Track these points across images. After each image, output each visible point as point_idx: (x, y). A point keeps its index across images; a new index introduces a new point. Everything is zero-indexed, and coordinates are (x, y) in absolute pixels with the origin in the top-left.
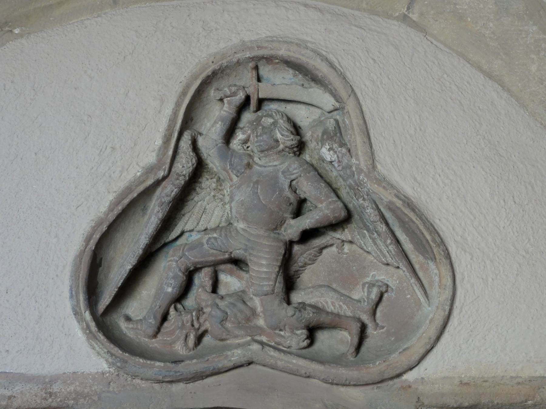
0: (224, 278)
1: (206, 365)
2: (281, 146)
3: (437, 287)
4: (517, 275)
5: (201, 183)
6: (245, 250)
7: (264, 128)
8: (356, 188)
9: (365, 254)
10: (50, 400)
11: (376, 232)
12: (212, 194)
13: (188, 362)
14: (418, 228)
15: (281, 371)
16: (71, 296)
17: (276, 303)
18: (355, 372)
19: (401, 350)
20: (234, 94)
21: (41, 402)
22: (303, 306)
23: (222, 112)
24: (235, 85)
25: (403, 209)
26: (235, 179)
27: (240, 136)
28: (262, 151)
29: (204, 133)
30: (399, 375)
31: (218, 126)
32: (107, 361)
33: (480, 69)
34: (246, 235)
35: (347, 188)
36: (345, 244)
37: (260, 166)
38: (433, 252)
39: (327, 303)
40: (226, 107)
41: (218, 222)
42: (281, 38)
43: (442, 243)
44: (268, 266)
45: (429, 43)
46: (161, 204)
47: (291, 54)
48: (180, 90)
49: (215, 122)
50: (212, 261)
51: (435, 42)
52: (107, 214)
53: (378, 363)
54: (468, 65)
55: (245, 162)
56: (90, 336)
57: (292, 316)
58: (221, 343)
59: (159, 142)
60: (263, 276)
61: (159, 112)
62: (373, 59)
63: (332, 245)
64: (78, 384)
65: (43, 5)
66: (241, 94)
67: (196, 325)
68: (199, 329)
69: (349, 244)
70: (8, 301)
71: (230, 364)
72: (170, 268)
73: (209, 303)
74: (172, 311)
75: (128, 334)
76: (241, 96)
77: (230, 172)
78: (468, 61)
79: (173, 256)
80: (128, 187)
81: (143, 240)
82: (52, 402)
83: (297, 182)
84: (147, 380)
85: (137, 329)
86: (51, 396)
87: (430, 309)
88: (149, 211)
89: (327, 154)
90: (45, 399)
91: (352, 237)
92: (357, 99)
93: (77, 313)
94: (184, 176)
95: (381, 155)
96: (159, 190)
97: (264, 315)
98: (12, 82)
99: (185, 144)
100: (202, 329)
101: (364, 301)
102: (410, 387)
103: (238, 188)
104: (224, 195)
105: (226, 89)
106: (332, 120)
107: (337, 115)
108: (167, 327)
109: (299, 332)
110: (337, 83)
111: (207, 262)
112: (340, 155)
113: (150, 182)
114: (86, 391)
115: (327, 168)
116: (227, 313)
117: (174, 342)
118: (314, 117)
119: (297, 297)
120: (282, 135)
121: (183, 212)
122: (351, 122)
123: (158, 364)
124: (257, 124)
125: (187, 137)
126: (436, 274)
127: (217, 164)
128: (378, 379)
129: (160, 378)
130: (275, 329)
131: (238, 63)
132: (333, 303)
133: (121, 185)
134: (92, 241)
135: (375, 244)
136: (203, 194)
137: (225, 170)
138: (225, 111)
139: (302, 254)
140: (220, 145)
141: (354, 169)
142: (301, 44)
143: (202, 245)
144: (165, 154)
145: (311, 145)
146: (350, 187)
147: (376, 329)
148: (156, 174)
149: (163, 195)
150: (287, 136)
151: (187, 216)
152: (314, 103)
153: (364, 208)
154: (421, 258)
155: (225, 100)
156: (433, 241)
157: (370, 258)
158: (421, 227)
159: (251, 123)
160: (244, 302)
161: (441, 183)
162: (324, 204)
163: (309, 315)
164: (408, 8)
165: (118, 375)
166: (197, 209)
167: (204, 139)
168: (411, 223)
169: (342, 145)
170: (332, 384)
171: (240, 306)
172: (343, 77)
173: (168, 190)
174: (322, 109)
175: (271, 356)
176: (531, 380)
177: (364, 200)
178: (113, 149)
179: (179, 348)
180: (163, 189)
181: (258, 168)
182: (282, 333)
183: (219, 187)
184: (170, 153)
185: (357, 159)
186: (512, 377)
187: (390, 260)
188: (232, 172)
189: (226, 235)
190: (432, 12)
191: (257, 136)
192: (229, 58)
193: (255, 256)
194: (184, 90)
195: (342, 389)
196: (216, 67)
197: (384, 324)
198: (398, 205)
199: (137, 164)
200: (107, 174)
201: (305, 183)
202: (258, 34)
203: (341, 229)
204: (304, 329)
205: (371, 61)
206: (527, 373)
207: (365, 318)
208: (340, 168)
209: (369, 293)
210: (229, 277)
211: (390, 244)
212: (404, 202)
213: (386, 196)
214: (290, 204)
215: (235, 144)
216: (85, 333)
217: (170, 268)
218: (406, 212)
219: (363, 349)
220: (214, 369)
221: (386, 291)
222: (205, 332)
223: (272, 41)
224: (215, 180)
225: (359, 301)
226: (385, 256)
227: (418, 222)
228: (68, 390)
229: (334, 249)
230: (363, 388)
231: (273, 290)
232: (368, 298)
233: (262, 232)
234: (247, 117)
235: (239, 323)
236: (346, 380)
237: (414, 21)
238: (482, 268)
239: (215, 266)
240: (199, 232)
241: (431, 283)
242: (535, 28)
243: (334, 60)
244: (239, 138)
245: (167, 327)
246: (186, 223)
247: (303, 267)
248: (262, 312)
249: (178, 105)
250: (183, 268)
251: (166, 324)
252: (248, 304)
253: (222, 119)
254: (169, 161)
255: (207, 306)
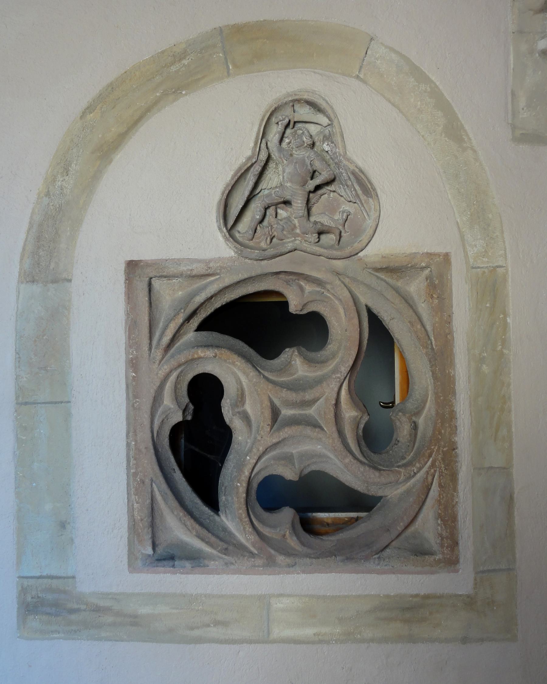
0: (279, 211)
1: (277, 251)
2: (306, 145)
3: (373, 210)
4: (405, 204)
5: (269, 165)
6: (291, 196)
7: (298, 135)
8: (338, 164)
9: (340, 197)
10: (209, 270)
11: (346, 185)
12: (274, 170)
13: (269, 250)
14: (365, 182)
15: (308, 253)
16: (217, 221)
17: (305, 220)
18: (340, 253)
19: (358, 241)
20: (284, 119)
21: (205, 272)
22: (316, 223)
23: (278, 129)
24: (284, 115)
25: (359, 173)
26: (285, 162)
27: (287, 140)
28: (297, 147)
29: (270, 140)
30: (357, 254)
31: (277, 136)
32: (234, 251)
33: (390, 102)
34: (291, 189)
35: (334, 164)
36: (331, 193)
37: (297, 155)
38: (371, 194)
39: (324, 221)
40: (280, 126)
41: (276, 185)
42: (305, 89)
43: (374, 190)
44: (301, 203)
45: (368, 89)
46: (254, 175)
47: (309, 97)
48: (261, 118)
49: (275, 134)
50: (276, 202)
51: (371, 89)
52: (230, 181)
53: (349, 248)
54: (385, 100)
55: (290, 153)
56: (226, 239)
57: (312, 227)
58: (281, 242)
59: (252, 145)
60: (299, 208)
61: (252, 130)
62: (345, 99)
63: (326, 193)
64: (221, 262)
65: (195, 78)
66: (287, 119)
67: (271, 234)
68: (272, 235)
69: (333, 192)
70: (188, 225)
71: (288, 250)
72: (257, 207)
73: (275, 223)
74: (258, 228)
75: (240, 240)
76: (287, 120)
77: (283, 159)
78: (384, 97)
79: (259, 201)
80: (239, 167)
81: (247, 193)
82: (210, 271)
83: (313, 162)
84: (251, 259)
85: (244, 236)
86: (209, 269)
87: (370, 221)
88: (247, 180)
89: (326, 147)
90: (207, 270)
91: (335, 189)
92: (338, 119)
93: (220, 229)
94: (264, 161)
95: (349, 148)
96: (252, 169)
97: (300, 227)
98: (184, 118)
99: (263, 146)
100: (273, 235)
101: (340, 220)
102: (361, 259)
103: (287, 166)
104: (279, 171)
105: (280, 117)
106: (327, 130)
107: (329, 128)
108: (257, 235)
109: (314, 235)
110: (330, 112)
111: (274, 203)
112: (332, 148)
113: (249, 164)
114: (225, 265)
115: (325, 155)
116: (284, 227)
117: (261, 242)
118: (317, 130)
119: (312, 219)
120: (306, 139)
121: (261, 180)
122: (336, 131)
123: (256, 251)
124: (295, 134)
125: (264, 141)
126: (373, 204)
127: (277, 155)
128: (349, 255)
129: (257, 258)
130: (304, 234)
131: (286, 103)
132: (327, 221)
133: (236, 167)
134: (225, 194)
135: (345, 191)
136: (270, 170)
137: (280, 158)
138: (280, 128)
139: (313, 198)
140: (278, 145)
141: (338, 154)
142: (314, 92)
143: (272, 194)
144: (255, 150)
145: (317, 144)
146: (336, 163)
147: (345, 233)
148: (252, 161)
149: (255, 171)
150: (309, 139)
151: (263, 181)
152: (319, 122)
153: (342, 173)
154: (365, 197)
155: (280, 123)
156: (371, 188)
157: (342, 199)
158: (367, 182)
159: (292, 133)
160: (291, 222)
161: (373, 160)
162: (325, 172)
163: (319, 226)
164: (359, 72)
165: (238, 258)
166: (267, 178)
167: (271, 143)
168: (362, 180)
169: (332, 142)
170: (330, 258)
171: (289, 223)
172: (332, 108)
173: (257, 168)
174: (322, 125)
175: (305, 246)
176: (411, 254)
177: (342, 169)
178: (232, 149)
179: (263, 245)
180: (254, 168)
181: (295, 156)
182: (307, 236)
183: (277, 167)
184: (258, 150)
185: (339, 149)
186: (403, 253)
187: (352, 199)
188: (284, 158)
189: (282, 189)
190: (369, 73)
191: (295, 140)
192: (282, 101)
193: (296, 199)
194: (262, 118)
195: (334, 261)
196: (276, 106)
197: (349, 231)
198: (356, 171)
199: (243, 156)
200: (229, 162)
201: (317, 162)
202: (294, 88)
203: (331, 185)
204: (316, 233)
205: (344, 100)
206: (408, 252)
207: (341, 228)
208: (332, 154)
209: (342, 216)
210: (282, 211)
211: (353, 191)
212: (359, 169)
213: (352, 167)
214: (310, 173)
215: (284, 145)
216: (224, 238)
217: (257, 207)
218: (360, 174)
219: (341, 242)
220: (281, 253)
221: (349, 215)
222: (274, 236)
223: (301, 91)
224: (275, 163)
225: (338, 220)
226: (349, 197)
227: (365, 179)
228: (217, 265)
229: (326, 195)
230: (342, 260)
231: (304, 215)
232: (342, 218)
233: (298, 187)
234: (289, 131)
235: (289, 231)
236: (336, 256)
237: (362, 79)
238: (391, 201)
239: (276, 205)
240: (268, 189)
241: (370, 209)
242: (413, 79)
243: (328, 99)
244: (286, 142)
245: (257, 235)
246: (263, 185)
247: (313, 205)
248: (299, 226)
249: (260, 126)
250: (263, 206)
251: (256, 234)
252: (293, 222)
253: (279, 132)
254: (257, 154)
255: (274, 224)
